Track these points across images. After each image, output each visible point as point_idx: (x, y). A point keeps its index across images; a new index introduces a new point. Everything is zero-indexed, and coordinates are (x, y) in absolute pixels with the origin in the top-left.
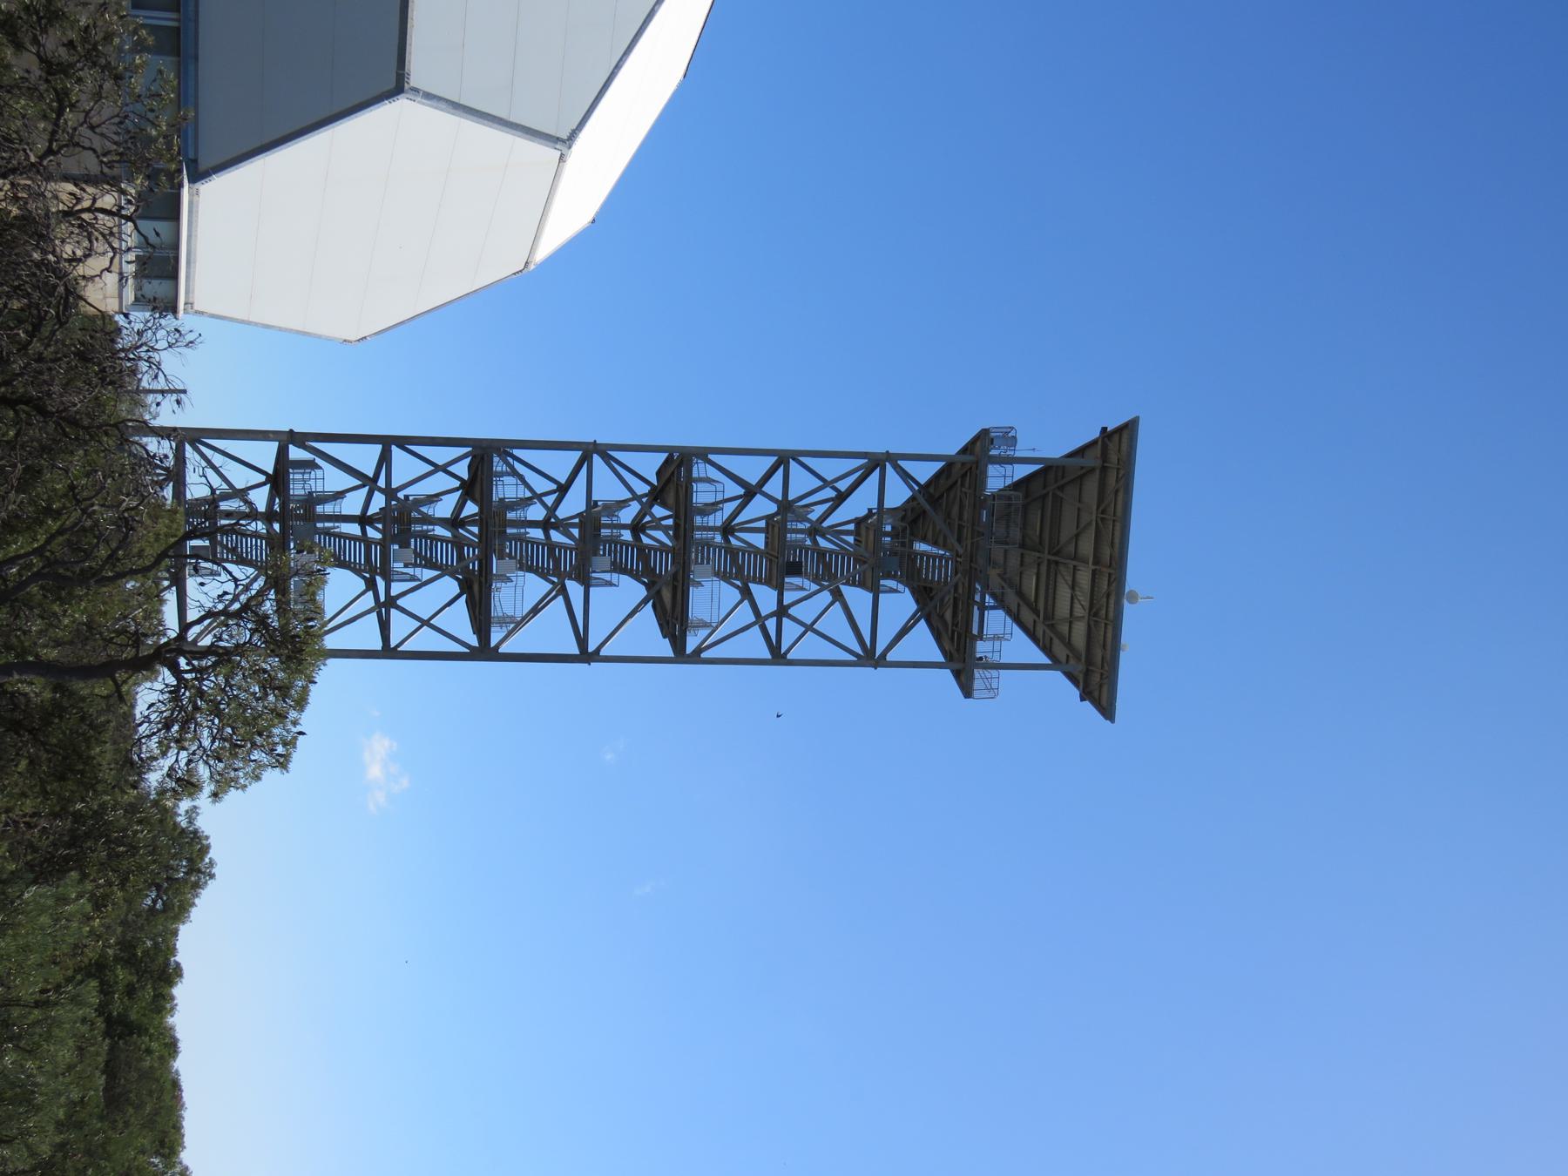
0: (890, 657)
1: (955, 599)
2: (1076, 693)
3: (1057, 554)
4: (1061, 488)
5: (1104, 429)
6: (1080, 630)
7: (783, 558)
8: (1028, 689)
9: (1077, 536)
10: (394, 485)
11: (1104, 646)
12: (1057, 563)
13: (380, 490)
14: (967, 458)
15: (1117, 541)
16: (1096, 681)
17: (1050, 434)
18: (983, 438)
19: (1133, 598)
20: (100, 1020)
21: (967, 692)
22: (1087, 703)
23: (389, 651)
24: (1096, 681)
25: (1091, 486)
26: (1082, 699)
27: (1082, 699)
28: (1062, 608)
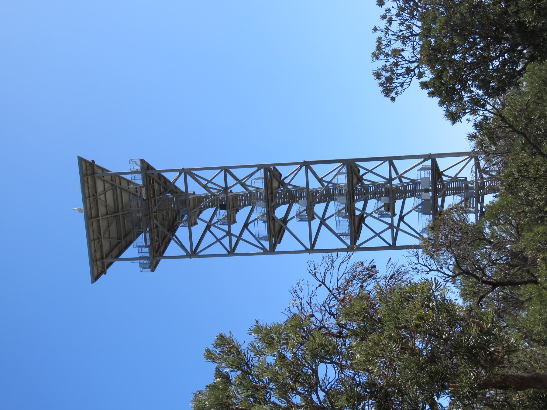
0: (178, 174)
1: (154, 197)
2: (97, 163)
3: (116, 216)
4: (119, 243)
5: (105, 274)
6: (100, 188)
7: (229, 203)
8: (118, 161)
9: (109, 226)
10: (390, 230)
11: (88, 187)
12: (115, 212)
13: (395, 227)
14: (158, 259)
15: (91, 232)
16: (89, 171)
17: (125, 271)
18: (153, 267)
19: (80, 210)
20: (535, 229)
21: (142, 161)
22: (90, 160)
23: (390, 160)
24: (89, 171)
25: (106, 246)
26: (93, 161)
27: (93, 161)
28: (109, 194)
